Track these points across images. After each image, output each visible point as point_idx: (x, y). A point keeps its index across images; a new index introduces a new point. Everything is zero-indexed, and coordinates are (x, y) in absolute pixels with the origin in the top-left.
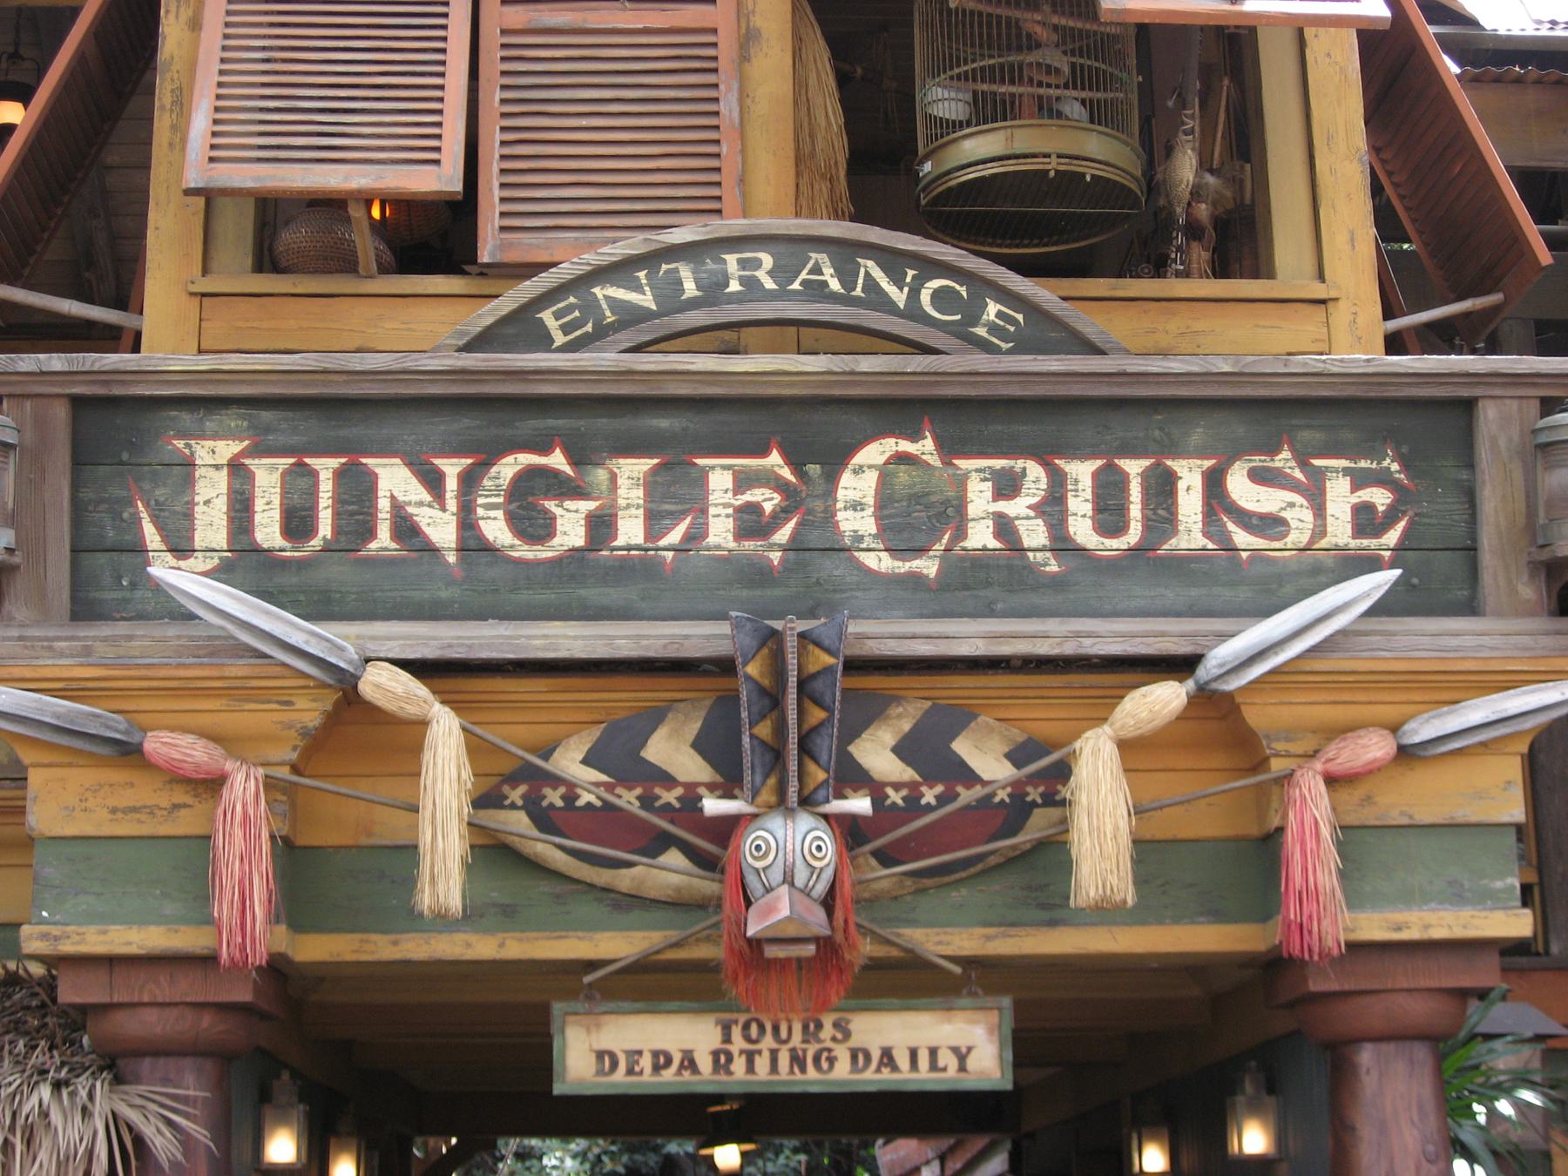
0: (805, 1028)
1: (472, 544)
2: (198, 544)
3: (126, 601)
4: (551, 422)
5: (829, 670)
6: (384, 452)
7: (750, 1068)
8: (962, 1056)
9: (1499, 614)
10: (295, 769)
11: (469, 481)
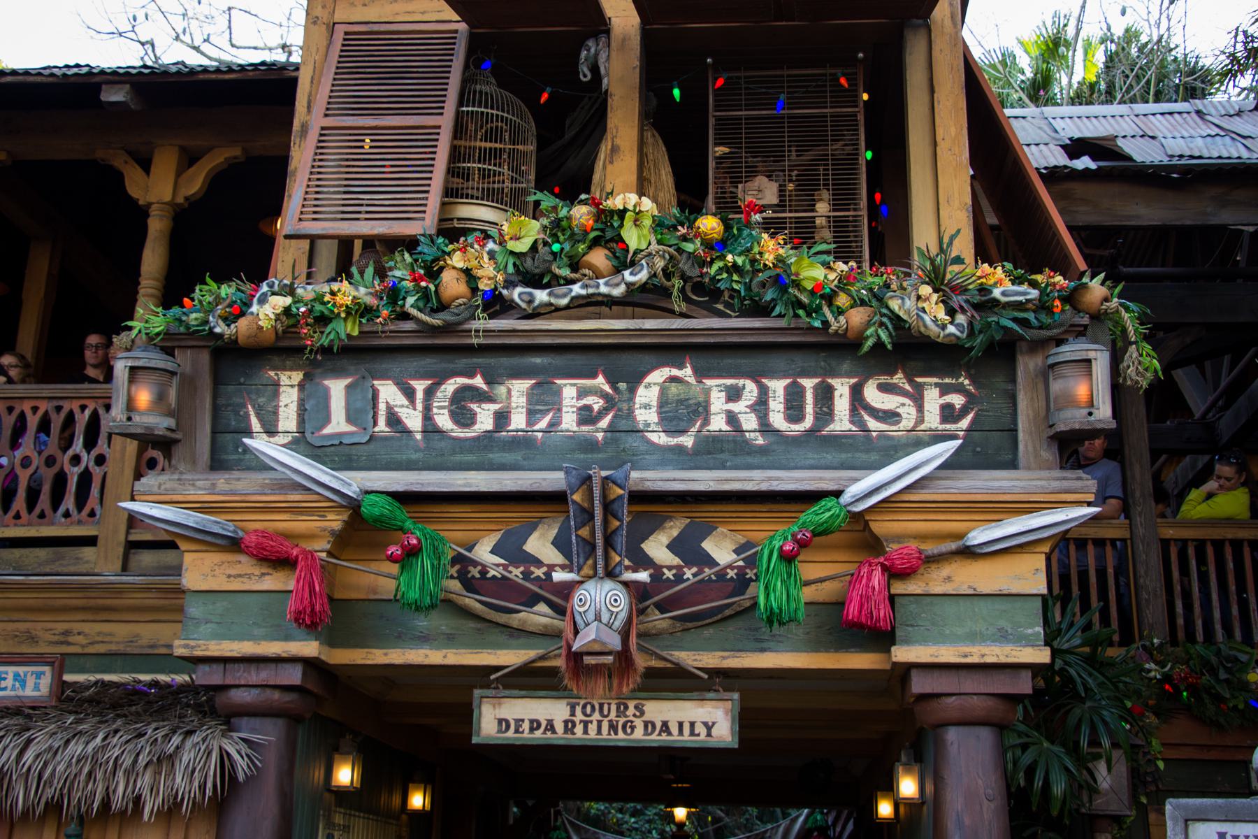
0: (618, 709)
1: (430, 428)
2: (280, 429)
3: (241, 460)
4: (475, 360)
5: (620, 497)
6: (383, 377)
7: (586, 732)
8: (709, 727)
9: (1028, 468)
10: (330, 553)
11: (429, 393)
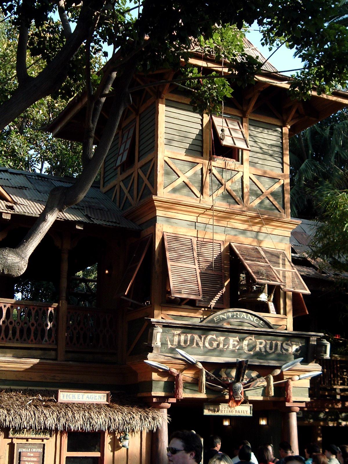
7: (224, 412)
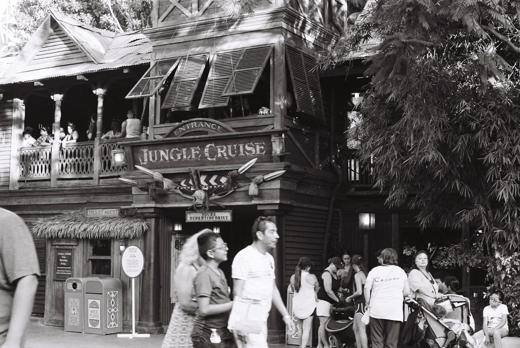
8: (227, 217)
